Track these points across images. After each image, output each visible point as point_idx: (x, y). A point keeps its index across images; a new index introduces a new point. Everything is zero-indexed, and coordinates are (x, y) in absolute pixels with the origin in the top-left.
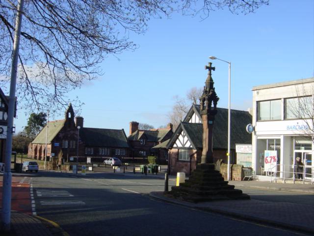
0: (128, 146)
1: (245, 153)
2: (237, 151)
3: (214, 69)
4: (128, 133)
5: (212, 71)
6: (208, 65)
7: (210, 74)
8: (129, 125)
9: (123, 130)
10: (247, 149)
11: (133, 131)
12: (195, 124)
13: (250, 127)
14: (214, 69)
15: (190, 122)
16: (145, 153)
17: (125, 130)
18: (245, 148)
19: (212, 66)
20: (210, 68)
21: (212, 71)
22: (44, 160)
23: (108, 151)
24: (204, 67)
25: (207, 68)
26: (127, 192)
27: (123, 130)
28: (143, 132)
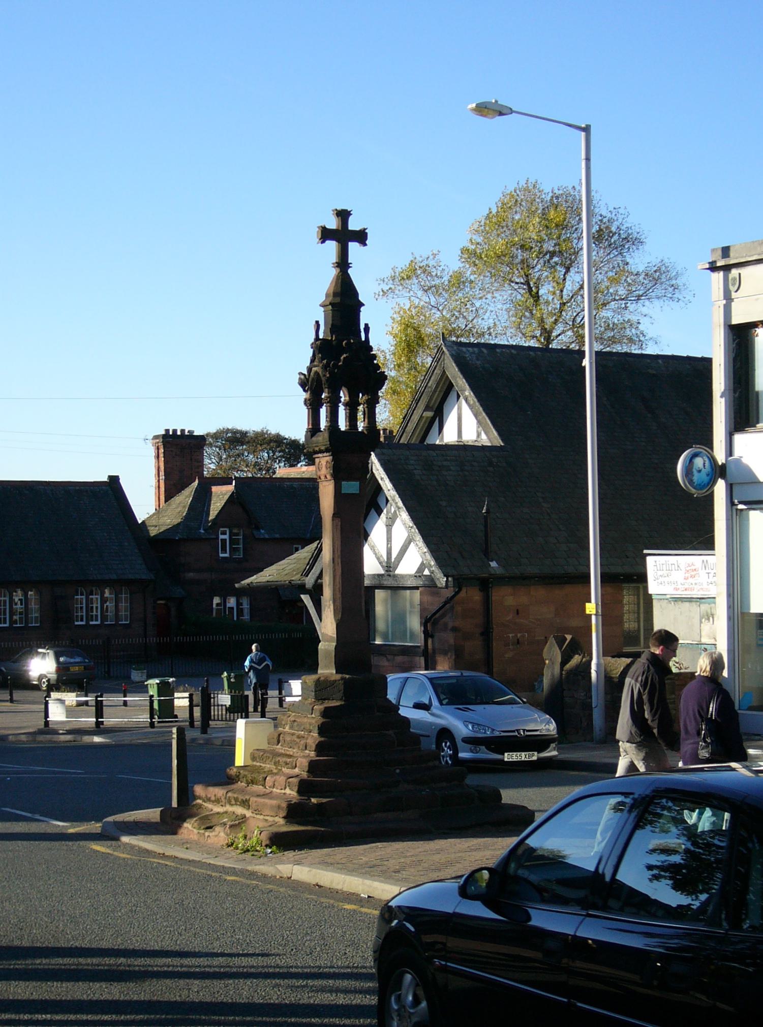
0: (145, 575)
1: (690, 600)
2: (653, 587)
3: (361, 237)
4: (144, 500)
5: (353, 247)
6: (333, 224)
7: (343, 264)
8: (152, 452)
9: (114, 480)
10: (703, 577)
11: (171, 486)
12: (462, 450)
13: (699, 462)
14: (361, 237)
15: (434, 439)
16: (246, 605)
17: (122, 482)
18: (692, 572)
19: (354, 225)
20: (343, 234)
21: (353, 247)
22: (614, 686)
23: (123, 605)
24: (315, 234)
25: (326, 234)
26: (149, 838)
27: (114, 480)
28: (231, 488)
